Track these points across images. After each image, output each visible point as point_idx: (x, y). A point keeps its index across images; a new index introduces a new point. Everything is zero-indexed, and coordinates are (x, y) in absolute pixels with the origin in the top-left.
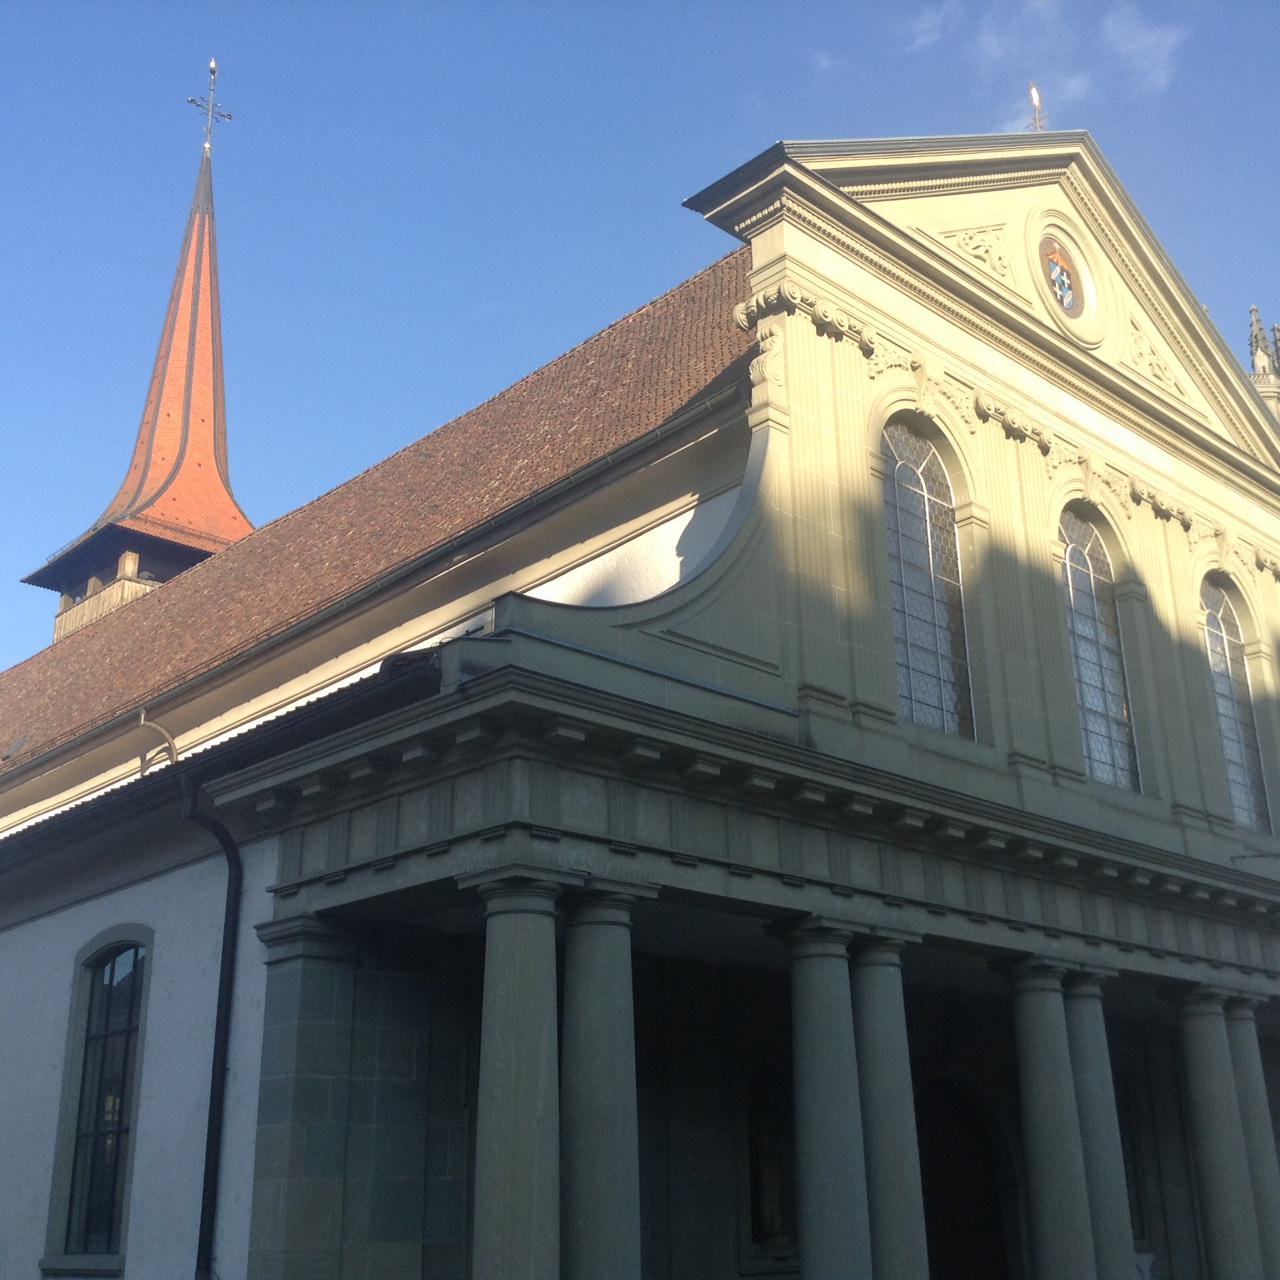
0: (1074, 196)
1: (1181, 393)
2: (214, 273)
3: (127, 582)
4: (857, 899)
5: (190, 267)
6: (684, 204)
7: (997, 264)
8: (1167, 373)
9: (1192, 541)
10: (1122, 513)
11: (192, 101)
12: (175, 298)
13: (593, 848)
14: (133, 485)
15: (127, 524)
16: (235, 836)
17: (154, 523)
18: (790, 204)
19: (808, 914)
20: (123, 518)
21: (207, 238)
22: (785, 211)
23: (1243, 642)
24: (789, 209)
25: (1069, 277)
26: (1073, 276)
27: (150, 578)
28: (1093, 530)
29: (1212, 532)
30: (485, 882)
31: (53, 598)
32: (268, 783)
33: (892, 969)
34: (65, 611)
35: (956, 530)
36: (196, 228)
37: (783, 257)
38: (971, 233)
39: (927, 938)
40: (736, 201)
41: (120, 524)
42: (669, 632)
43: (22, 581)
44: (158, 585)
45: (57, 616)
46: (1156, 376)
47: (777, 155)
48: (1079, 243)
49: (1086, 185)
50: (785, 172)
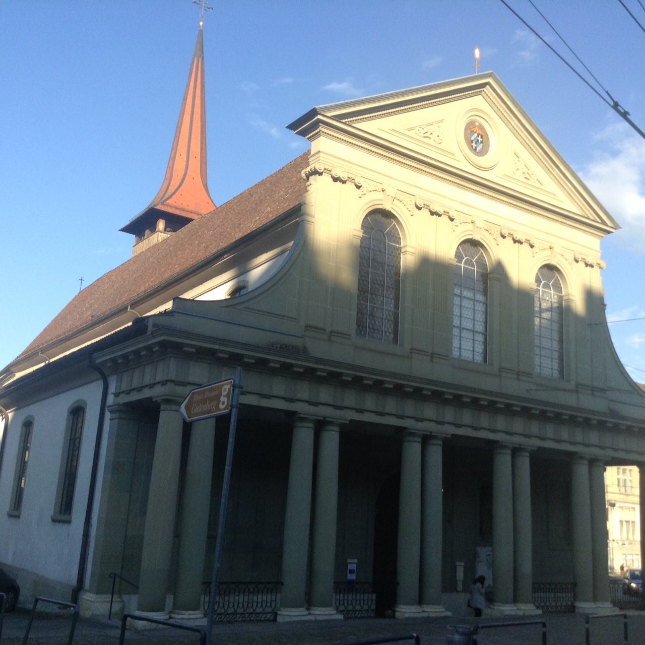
0: (489, 100)
1: (542, 185)
2: (203, 86)
3: (160, 233)
4: (321, 406)
5: (192, 84)
6: (287, 127)
7: (437, 139)
8: (533, 176)
9: (535, 252)
10: (494, 243)
11: (195, 2)
12: (185, 99)
14: (165, 188)
15: (159, 207)
16: (106, 372)
17: (171, 206)
18: (323, 130)
19: (297, 412)
20: (158, 204)
21: (200, 69)
22: (321, 132)
23: (563, 294)
24: (323, 132)
25: (482, 137)
26: (484, 137)
27: (170, 231)
28: (480, 250)
29: (548, 247)
30: (159, 399)
31: (132, 238)
32: (108, 357)
33: (333, 433)
34: (136, 244)
35: (401, 256)
36: (195, 65)
37: (319, 152)
38: (423, 127)
39: (351, 421)
40: (304, 128)
41: (156, 207)
42: (246, 308)
43: (120, 230)
44: (173, 233)
45: (134, 247)
46: (526, 178)
47: (314, 113)
48: (488, 120)
49: (494, 94)
50: (318, 118)
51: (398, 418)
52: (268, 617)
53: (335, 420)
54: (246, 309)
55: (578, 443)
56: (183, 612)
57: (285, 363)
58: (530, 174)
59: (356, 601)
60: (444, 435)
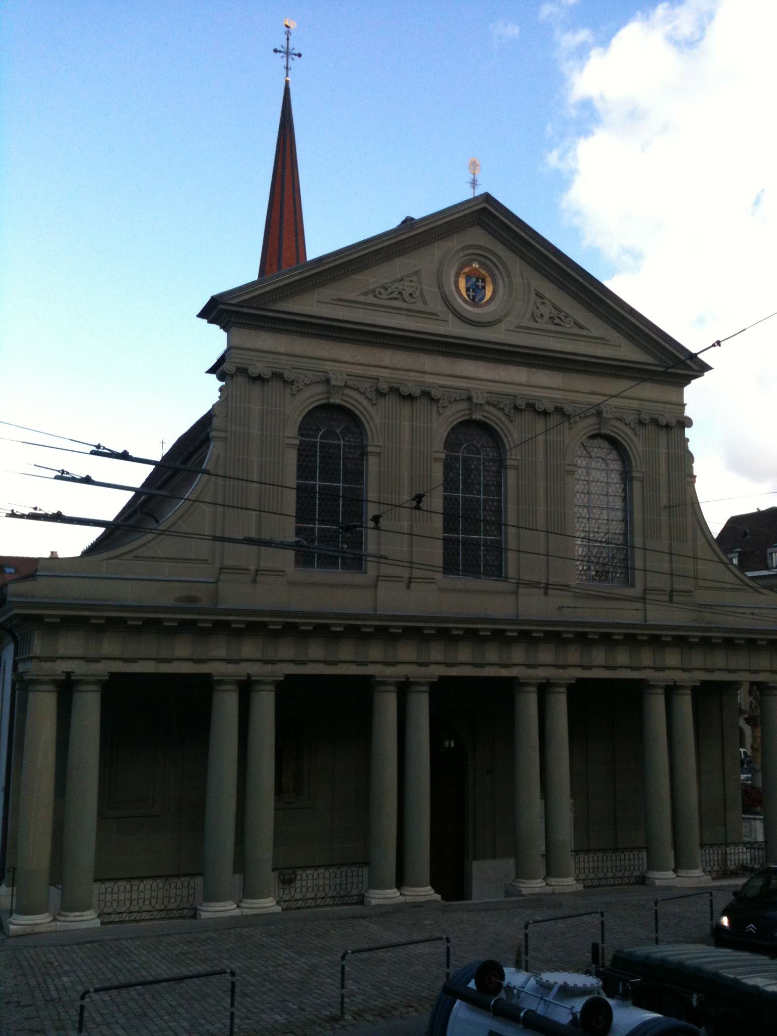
4: (594, 669)
13: (76, 662)
42: (136, 557)
51: (358, 665)
52: (134, 916)
53: (387, 679)
54: (136, 558)
55: (645, 668)
56: (69, 914)
57: (603, 633)
58: (563, 318)
59: (714, 862)
60: (395, 679)
